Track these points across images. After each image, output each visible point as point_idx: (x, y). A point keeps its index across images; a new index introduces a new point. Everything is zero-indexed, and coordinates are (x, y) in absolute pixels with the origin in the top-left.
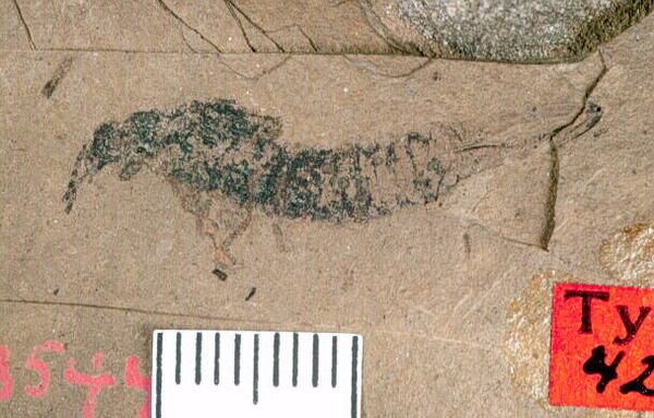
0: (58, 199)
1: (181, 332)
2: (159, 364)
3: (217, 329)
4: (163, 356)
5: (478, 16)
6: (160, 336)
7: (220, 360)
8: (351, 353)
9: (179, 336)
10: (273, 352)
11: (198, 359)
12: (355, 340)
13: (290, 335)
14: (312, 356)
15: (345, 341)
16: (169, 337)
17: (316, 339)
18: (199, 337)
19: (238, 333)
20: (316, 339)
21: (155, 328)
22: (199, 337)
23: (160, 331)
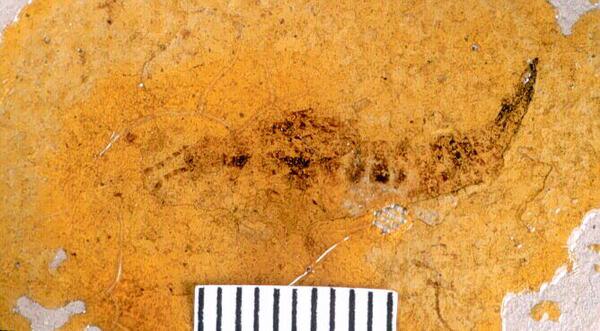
0: (587, 241)
1: (222, 286)
2: (201, 317)
3: (368, 287)
4: (204, 310)
5: (94, 202)
6: (202, 291)
7: (260, 314)
8: (298, 300)
9: (220, 291)
10: (310, 306)
11: (294, 312)
12: (390, 296)
13: (327, 290)
14: (348, 310)
15: (380, 297)
16: (210, 292)
17: (352, 294)
18: (239, 292)
19: (277, 287)
20: (352, 294)
21: (195, 284)
22: (239, 292)
23: (202, 287)
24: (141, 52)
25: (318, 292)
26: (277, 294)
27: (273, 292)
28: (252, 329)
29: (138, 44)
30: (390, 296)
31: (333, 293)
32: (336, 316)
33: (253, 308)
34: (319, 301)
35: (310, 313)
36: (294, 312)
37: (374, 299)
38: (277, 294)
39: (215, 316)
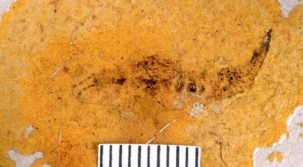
0: (296, 121)
1: (112, 145)
2: (101, 160)
3: (186, 145)
4: (103, 157)
5: (47, 102)
6: (102, 147)
7: (131, 158)
8: (150, 151)
9: (111, 147)
10: (157, 155)
11: (149, 158)
12: (197, 149)
13: (165, 146)
14: (176, 156)
15: (192, 150)
16: (106, 147)
17: (178, 148)
18: (121, 147)
19: (140, 145)
20: (178, 148)
21: (99, 143)
22: (121, 147)
23: (102, 145)
24: (71, 26)
25: (161, 147)
26: (140, 148)
27: (138, 147)
28: (127, 166)
29: (69, 22)
30: (197, 149)
31: (168, 148)
32: (170, 160)
33: (128, 155)
34: (161, 152)
35: (157, 158)
36: (149, 158)
37: (189, 151)
38: (140, 148)
39: (109, 159)
